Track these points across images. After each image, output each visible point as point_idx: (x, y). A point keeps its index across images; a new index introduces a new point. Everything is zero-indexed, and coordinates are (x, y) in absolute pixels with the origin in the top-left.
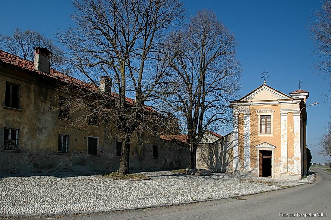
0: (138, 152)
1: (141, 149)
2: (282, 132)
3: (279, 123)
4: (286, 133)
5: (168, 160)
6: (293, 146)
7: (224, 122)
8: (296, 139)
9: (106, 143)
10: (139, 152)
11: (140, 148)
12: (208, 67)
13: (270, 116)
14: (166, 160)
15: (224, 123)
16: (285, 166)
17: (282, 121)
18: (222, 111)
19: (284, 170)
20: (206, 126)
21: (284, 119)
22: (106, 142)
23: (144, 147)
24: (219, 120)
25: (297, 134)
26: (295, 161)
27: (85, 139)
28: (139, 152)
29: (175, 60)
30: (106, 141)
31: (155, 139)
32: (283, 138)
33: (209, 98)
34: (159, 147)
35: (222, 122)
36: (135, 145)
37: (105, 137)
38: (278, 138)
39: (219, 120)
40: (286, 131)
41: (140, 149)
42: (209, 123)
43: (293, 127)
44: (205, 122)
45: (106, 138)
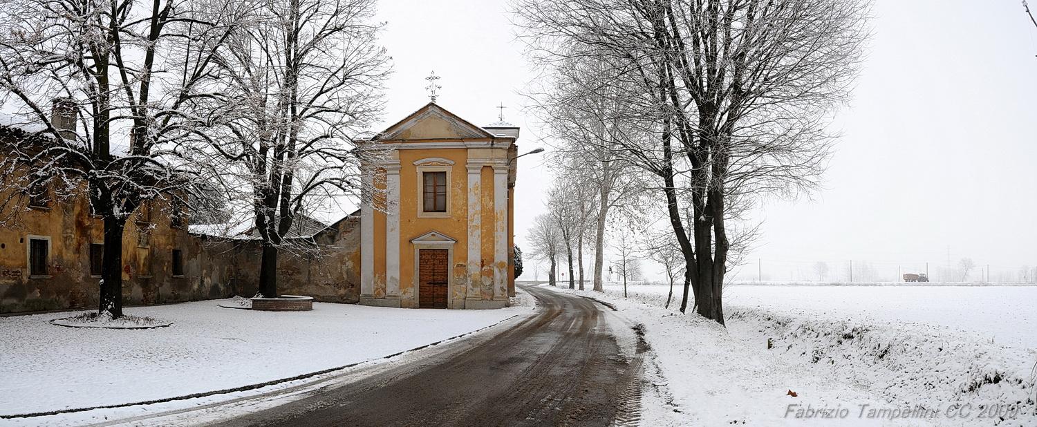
0: (139, 265)
1: (145, 258)
2: (469, 207)
3: (465, 190)
4: (479, 212)
5: (207, 281)
6: (491, 239)
7: (343, 186)
8: (499, 223)
9: (66, 248)
10: (142, 266)
11: (143, 254)
12: (306, 60)
13: (517, 130)
14: (202, 281)
15: (344, 190)
16: (476, 282)
17: (470, 185)
18: (340, 163)
19: (472, 290)
20: (300, 198)
21: (474, 179)
22: (66, 245)
23: (152, 253)
24: (333, 183)
25: (501, 214)
26: (496, 270)
27: (22, 241)
28: (142, 266)
29: (224, 51)
30: (68, 243)
31: (177, 234)
32: (472, 221)
33: (312, 128)
34: (185, 254)
35: (340, 186)
36: (131, 249)
37: (65, 235)
38: (463, 221)
39: (333, 183)
40: (479, 208)
41: (143, 257)
42: (307, 189)
43: (492, 198)
44: (297, 187)
45: (66, 238)
